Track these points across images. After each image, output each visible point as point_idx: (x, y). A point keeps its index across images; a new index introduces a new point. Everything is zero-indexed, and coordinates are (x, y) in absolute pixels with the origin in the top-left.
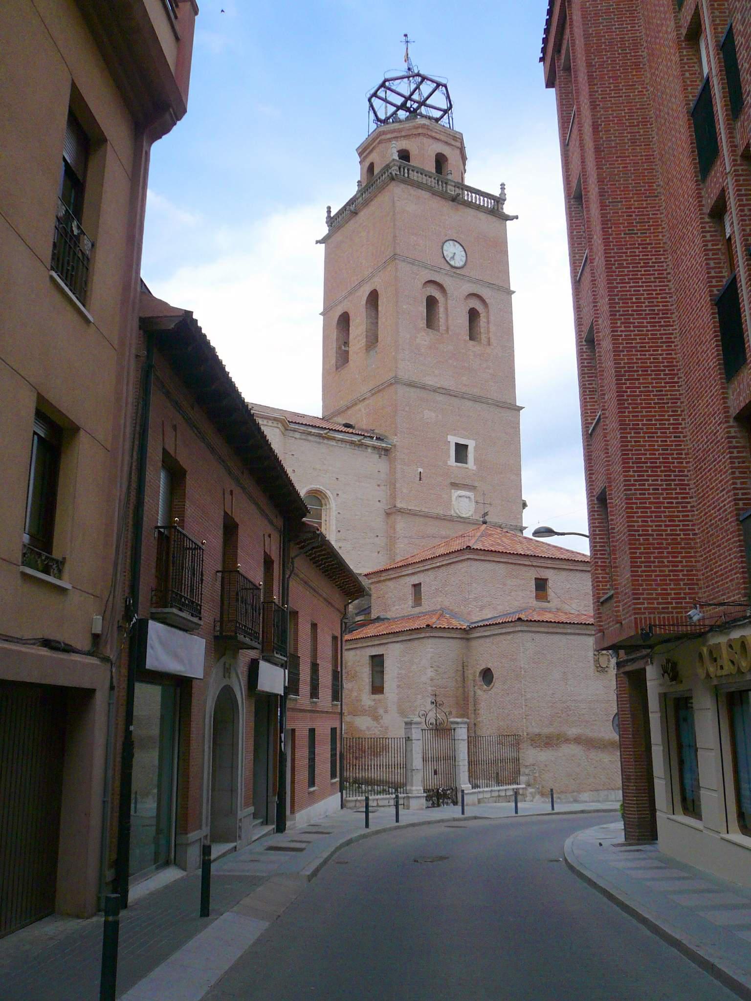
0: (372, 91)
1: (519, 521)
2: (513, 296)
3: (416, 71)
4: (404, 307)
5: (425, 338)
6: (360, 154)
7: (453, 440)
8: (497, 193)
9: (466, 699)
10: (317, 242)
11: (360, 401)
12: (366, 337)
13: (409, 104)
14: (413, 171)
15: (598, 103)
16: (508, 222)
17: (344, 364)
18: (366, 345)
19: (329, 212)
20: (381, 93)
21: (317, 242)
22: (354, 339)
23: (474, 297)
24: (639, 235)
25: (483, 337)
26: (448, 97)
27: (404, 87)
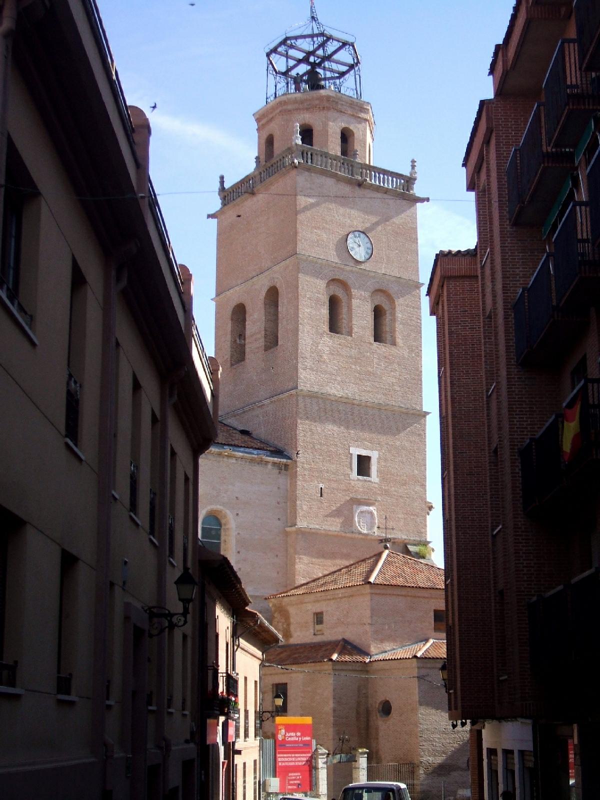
0: (272, 46)
1: (424, 535)
5: (328, 342)
6: (258, 120)
7: (356, 451)
8: (406, 172)
9: (368, 727)
10: (209, 216)
12: (265, 338)
14: (316, 154)
15: (455, 382)
16: (419, 205)
19: (222, 182)
21: (209, 216)
22: (252, 336)
24: (476, 475)
25: (388, 337)
27: (307, 45)
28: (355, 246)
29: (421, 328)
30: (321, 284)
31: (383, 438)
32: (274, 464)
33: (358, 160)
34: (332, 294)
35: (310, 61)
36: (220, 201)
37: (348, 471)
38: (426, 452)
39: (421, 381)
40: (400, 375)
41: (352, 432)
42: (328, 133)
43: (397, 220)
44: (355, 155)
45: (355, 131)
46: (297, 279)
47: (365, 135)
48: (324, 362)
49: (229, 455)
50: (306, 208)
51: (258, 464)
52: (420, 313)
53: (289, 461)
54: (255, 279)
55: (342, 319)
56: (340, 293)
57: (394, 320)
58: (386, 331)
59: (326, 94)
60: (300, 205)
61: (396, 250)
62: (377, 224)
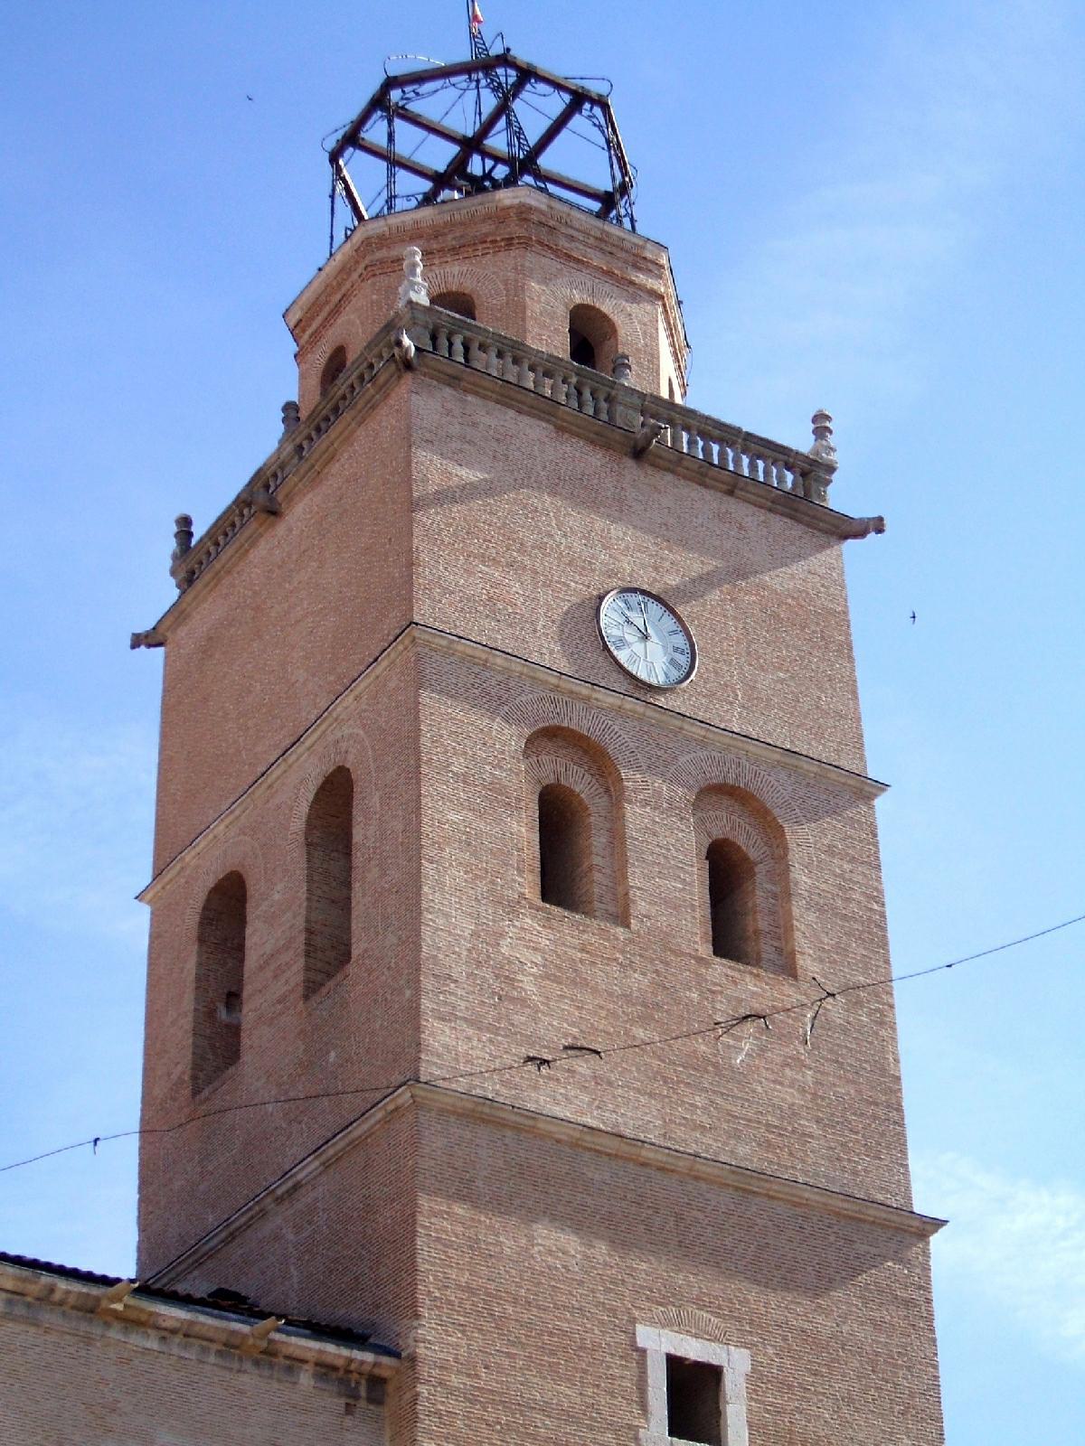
2: (879, 803)
3: (496, 50)
4: (452, 816)
6: (296, 330)
7: (659, 1342)
8: (800, 440)
10: (137, 641)
11: (279, 1200)
12: (307, 954)
13: (476, 166)
16: (850, 545)
17: (219, 1070)
18: (307, 981)
20: (375, 132)
21: (137, 641)
22: (261, 968)
23: (726, 801)
25: (767, 949)
26: (614, 147)
28: (631, 636)
29: (884, 929)
30: (510, 738)
31: (772, 1304)
32: (325, 1370)
33: (631, 380)
34: (551, 780)
35: (469, 170)
36: (171, 562)
37: (631, 1415)
38: (936, 1367)
39: (899, 1109)
40: (818, 1083)
41: (644, 1266)
42: (524, 312)
43: (783, 579)
44: (620, 365)
45: (618, 319)
46: (414, 712)
47: (655, 339)
48: (523, 1002)
49: (133, 1315)
50: (445, 497)
51: (257, 1363)
52: (879, 879)
53: (385, 1360)
54: (275, 773)
55: (590, 869)
56: (580, 783)
57: (785, 894)
58: (757, 932)
59: (516, 201)
60: (425, 480)
61: (780, 669)
62: (707, 581)
